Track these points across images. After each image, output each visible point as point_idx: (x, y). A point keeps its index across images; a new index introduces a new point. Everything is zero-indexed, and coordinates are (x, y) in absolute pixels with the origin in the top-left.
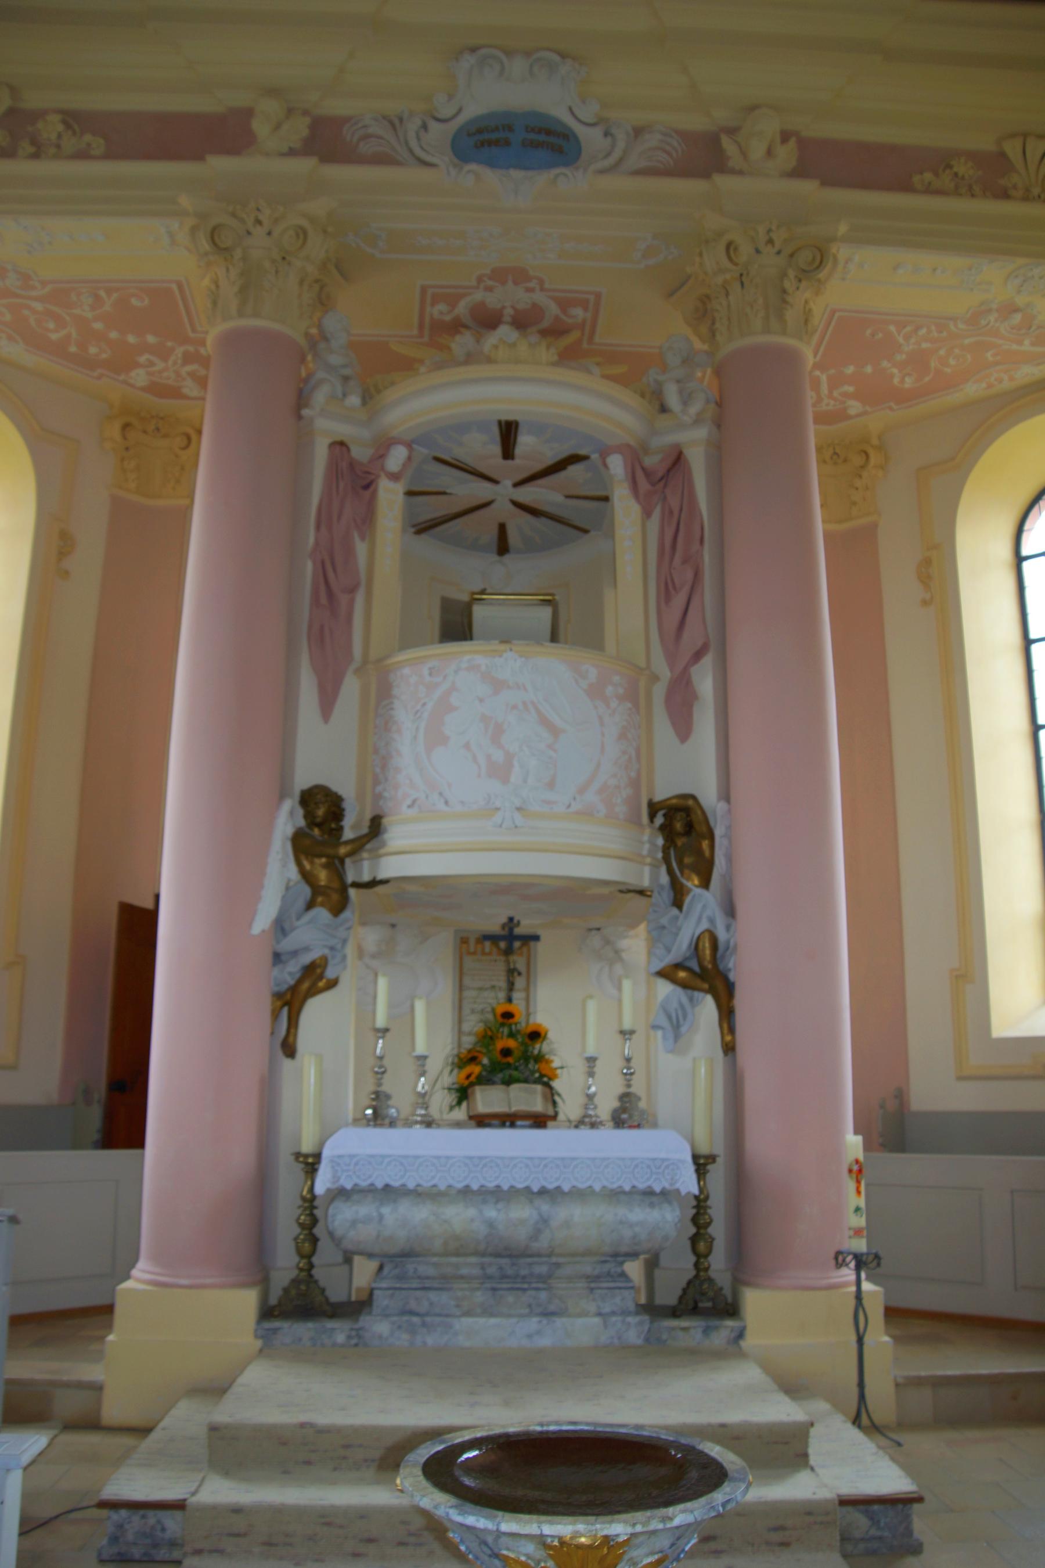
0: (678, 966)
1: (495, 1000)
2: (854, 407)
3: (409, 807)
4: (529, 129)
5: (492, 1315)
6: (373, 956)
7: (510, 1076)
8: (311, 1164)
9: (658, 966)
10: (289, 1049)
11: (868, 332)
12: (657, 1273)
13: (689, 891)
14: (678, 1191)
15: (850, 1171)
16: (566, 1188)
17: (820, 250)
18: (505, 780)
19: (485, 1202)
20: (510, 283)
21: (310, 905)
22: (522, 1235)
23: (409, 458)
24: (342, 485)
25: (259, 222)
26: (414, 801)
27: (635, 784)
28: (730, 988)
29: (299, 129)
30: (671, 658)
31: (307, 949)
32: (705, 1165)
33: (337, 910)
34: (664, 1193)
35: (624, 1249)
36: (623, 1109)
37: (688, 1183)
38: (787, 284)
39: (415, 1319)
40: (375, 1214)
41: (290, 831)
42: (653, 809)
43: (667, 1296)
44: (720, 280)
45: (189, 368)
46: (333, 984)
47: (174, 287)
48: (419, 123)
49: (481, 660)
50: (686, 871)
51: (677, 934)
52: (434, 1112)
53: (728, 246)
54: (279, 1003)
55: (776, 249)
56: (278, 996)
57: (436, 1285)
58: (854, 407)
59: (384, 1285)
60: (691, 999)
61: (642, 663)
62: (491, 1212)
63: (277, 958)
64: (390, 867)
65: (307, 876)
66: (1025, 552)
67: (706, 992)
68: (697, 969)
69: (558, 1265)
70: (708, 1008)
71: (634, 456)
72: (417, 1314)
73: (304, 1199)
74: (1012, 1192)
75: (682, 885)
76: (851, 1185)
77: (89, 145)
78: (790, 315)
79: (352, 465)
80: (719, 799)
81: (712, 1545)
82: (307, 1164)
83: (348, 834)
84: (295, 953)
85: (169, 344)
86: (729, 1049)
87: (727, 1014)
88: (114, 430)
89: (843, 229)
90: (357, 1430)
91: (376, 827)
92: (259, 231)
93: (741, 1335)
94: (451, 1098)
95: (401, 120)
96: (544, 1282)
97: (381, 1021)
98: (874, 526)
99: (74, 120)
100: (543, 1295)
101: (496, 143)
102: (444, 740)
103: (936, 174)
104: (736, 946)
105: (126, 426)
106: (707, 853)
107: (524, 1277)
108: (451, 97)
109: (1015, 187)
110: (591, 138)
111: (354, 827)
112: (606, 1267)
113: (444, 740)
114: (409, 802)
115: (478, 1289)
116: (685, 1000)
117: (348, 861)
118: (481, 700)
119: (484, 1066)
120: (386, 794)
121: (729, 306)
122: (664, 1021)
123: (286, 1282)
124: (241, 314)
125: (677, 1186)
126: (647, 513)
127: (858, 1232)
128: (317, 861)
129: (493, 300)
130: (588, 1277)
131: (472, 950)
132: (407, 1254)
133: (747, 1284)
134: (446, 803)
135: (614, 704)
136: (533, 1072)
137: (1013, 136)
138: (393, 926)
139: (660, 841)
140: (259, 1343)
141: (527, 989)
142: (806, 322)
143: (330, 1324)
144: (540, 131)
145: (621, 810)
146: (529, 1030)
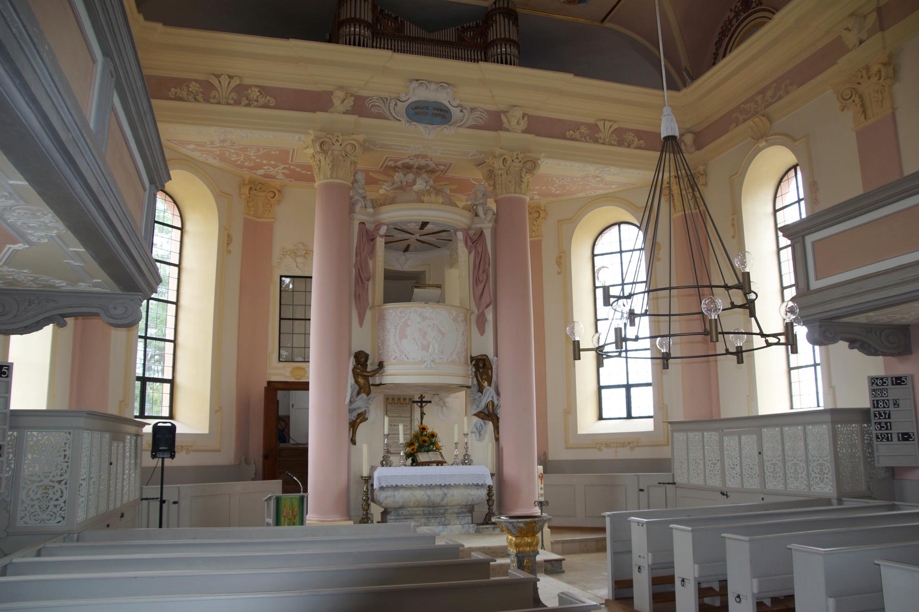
0: (480, 412)
2: (537, 197)
3: (393, 359)
4: (434, 109)
5: (427, 526)
9: (475, 412)
10: (353, 441)
11: (546, 179)
13: (485, 387)
14: (486, 484)
16: (452, 484)
17: (534, 162)
18: (427, 351)
19: (427, 489)
21: (359, 393)
22: (438, 500)
24: (364, 239)
25: (337, 141)
26: (396, 357)
27: (466, 350)
28: (498, 419)
29: (350, 102)
30: (478, 308)
31: (359, 408)
33: (368, 394)
37: (489, 481)
38: (522, 175)
42: (472, 359)
44: (500, 172)
48: (394, 103)
49: (419, 310)
50: (484, 381)
51: (481, 402)
53: (504, 159)
56: (350, 424)
58: (537, 197)
60: (484, 423)
61: (469, 309)
62: (429, 492)
63: (351, 411)
64: (387, 380)
65: (357, 382)
66: (596, 253)
67: (490, 420)
68: (487, 413)
69: (447, 510)
70: (490, 425)
71: (466, 231)
74: (585, 486)
76: (540, 481)
78: (524, 186)
79: (367, 231)
80: (494, 356)
83: (369, 369)
85: (279, 164)
89: (543, 155)
91: (381, 365)
95: (387, 99)
98: (540, 241)
99: (263, 90)
100: (443, 519)
102: (406, 337)
103: (574, 132)
104: (500, 406)
105: (251, 188)
106: (490, 375)
109: (600, 138)
110: (456, 113)
111: (372, 364)
113: (406, 337)
114: (394, 357)
115: (422, 518)
116: (482, 423)
117: (370, 378)
118: (419, 323)
120: (384, 354)
121: (502, 180)
122: (475, 430)
124: (332, 178)
126: (470, 253)
127: (541, 495)
129: (411, 162)
130: (456, 513)
131: (391, 402)
132: (402, 507)
134: (407, 358)
135: (460, 323)
137: (601, 120)
139: (474, 370)
145: (463, 360)
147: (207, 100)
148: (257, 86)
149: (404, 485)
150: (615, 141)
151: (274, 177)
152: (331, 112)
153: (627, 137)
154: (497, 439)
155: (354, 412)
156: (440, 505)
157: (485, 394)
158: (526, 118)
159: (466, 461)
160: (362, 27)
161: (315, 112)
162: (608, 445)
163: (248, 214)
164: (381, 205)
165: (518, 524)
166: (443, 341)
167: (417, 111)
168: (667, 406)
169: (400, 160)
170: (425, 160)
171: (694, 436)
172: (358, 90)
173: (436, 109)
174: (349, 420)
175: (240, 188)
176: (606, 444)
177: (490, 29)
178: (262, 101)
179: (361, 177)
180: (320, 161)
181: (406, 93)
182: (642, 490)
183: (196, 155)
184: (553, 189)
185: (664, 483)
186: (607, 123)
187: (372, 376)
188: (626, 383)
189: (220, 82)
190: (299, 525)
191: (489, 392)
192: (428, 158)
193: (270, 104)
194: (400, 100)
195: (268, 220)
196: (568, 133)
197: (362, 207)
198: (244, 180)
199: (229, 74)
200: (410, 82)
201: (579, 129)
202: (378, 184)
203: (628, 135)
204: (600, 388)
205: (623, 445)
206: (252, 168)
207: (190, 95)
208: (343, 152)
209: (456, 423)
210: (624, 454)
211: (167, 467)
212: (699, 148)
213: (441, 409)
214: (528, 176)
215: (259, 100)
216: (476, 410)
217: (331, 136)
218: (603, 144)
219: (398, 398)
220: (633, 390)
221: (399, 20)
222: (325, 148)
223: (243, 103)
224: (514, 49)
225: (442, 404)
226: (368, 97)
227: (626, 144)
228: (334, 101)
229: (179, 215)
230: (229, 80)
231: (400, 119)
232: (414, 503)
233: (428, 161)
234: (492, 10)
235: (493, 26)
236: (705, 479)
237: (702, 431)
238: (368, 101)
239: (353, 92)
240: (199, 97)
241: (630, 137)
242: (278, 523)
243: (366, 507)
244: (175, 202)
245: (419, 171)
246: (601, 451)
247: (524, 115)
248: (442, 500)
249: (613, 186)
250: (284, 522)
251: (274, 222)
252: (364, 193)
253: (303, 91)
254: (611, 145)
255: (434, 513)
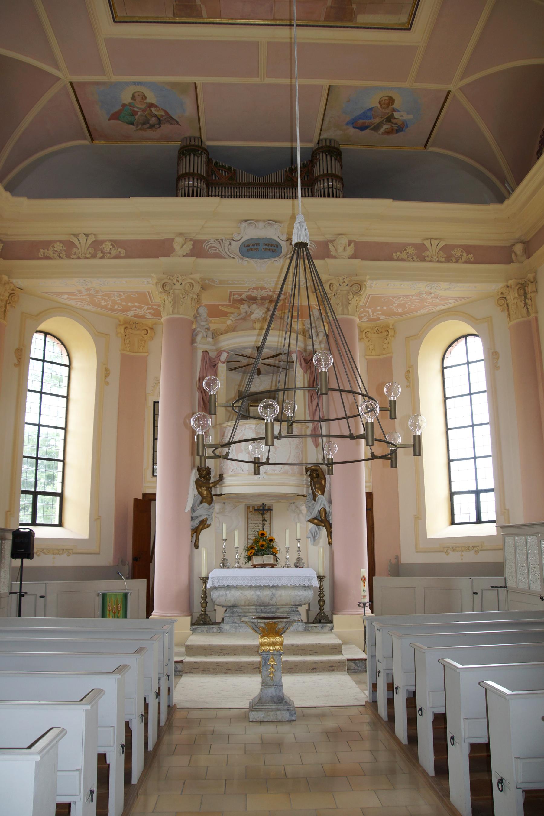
0: (315, 519)
1: (259, 529)
2: (382, 317)
3: (231, 472)
4: (265, 245)
6: (217, 513)
7: (263, 553)
8: (205, 580)
9: (309, 519)
10: (196, 546)
12: (309, 612)
13: (318, 495)
15: (362, 579)
19: (256, 590)
20: (259, 290)
21: (201, 502)
22: (267, 600)
23: (228, 356)
26: (233, 470)
29: (189, 246)
31: (201, 516)
32: (322, 579)
34: (308, 587)
35: (297, 603)
36: (297, 563)
37: (316, 583)
38: (349, 297)
39: (237, 625)
40: (225, 594)
41: (195, 479)
43: (312, 619)
45: (149, 311)
46: (209, 526)
47: (147, 292)
48: (229, 243)
52: (241, 564)
53: (331, 284)
54: (193, 532)
55: (346, 284)
56: (192, 530)
57: (243, 615)
58: (382, 317)
59: (227, 615)
60: (319, 529)
62: (258, 593)
63: (192, 519)
64: (226, 490)
65: (200, 493)
70: (324, 531)
72: (237, 623)
73: (203, 591)
75: (315, 494)
76: (362, 583)
77: (120, 252)
78: (350, 308)
81: (315, 670)
82: (203, 580)
83: (212, 480)
84: (197, 517)
85: (143, 305)
86: (330, 544)
87: (330, 533)
88: (122, 330)
89: (368, 277)
90: (224, 646)
92: (178, 284)
93: (332, 629)
94: (246, 560)
95: (222, 240)
96: (274, 614)
97: (224, 538)
98: (391, 357)
99: (115, 243)
101: (254, 250)
103: (401, 253)
105: (126, 328)
106: (323, 484)
107: (268, 612)
108: (239, 234)
109: (428, 257)
111: (214, 477)
112: (293, 609)
117: (212, 488)
119: (255, 550)
120: (224, 467)
122: (311, 536)
123: (198, 615)
124: (173, 314)
125: (312, 584)
128: (203, 488)
129: (254, 294)
132: (234, 606)
133: (335, 614)
134: (243, 471)
136: (270, 552)
137: (427, 239)
138: (224, 503)
139: (309, 479)
140: (191, 632)
141: (270, 524)
142: (357, 307)
143: (212, 626)
144: (268, 245)
146: (269, 539)
147: (69, 257)
148: (110, 241)
149: (235, 585)
150: (443, 258)
151: (143, 317)
152: (173, 257)
153: (455, 253)
154: (330, 544)
155: (197, 520)
156: (270, 604)
157: (317, 502)
158: (352, 245)
159: (298, 564)
160: (195, 180)
161: (158, 258)
162: (454, 549)
163: (124, 350)
164: (222, 334)
165: (259, 624)
166: (276, 454)
167: (250, 247)
168: (508, 510)
169: (243, 293)
170: (265, 292)
171: (520, 540)
172: (196, 235)
173: (266, 245)
174: (192, 527)
175: (117, 328)
176: (452, 548)
177: (314, 167)
178: (114, 252)
179: (203, 311)
180: (164, 300)
181: (238, 234)
182: (475, 593)
183: (72, 303)
184: (394, 308)
185: (496, 587)
186: (433, 241)
187: (213, 486)
188: (475, 489)
189: (79, 240)
190: (123, 618)
191: (322, 500)
192: (266, 289)
193: (121, 255)
194: (234, 240)
195: (388, 355)
196: (395, 254)
197: (203, 337)
198: (120, 321)
199: (85, 233)
200: (241, 223)
201: (406, 250)
202: (227, 316)
203: (456, 250)
204: (452, 494)
205: (468, 549)
206: (123, 311)
207: (55, 253)
208: (183, 291)
209: (287, 529)
210: (469, 558)
211: (25, 567)
212: (529, 257)
213: (298, 517)
214: (356, 298)
215: (111, 252)
216: (309, 517)
217: (171, 277)
218: (431, 261)
219: (253, 507)
220: (482, 495)
221: (232, 169)
222: (167, 287)
223: (98, 256)
224: (339, 185)
225: (298, 511)
226: (206, 240)
227: (454, 260)
228: (175, 246)
229: (67, 355)
230: (86, 238)
231: (234, 257)
232: (245, 602)
233: (267, 292)
234: (316, 150)
235: (317, 164)
236: (529, 583)
237: (526, 535)
238: (206, 244)
239: (191, 237)
240: (63, 255)
241: (458, 252)
242: (103, 616)
243: (204, 605)
244: (63, 344)
245: (263, 301)
246: (448, 554)
247: (350, 243)
248: (271, 600)
249: (451, 301)
250: (109, 615)
251: (148, 356)
252: (207, 325)
253: (149, 241)
254: (438, 262)
255: (266, 612)
